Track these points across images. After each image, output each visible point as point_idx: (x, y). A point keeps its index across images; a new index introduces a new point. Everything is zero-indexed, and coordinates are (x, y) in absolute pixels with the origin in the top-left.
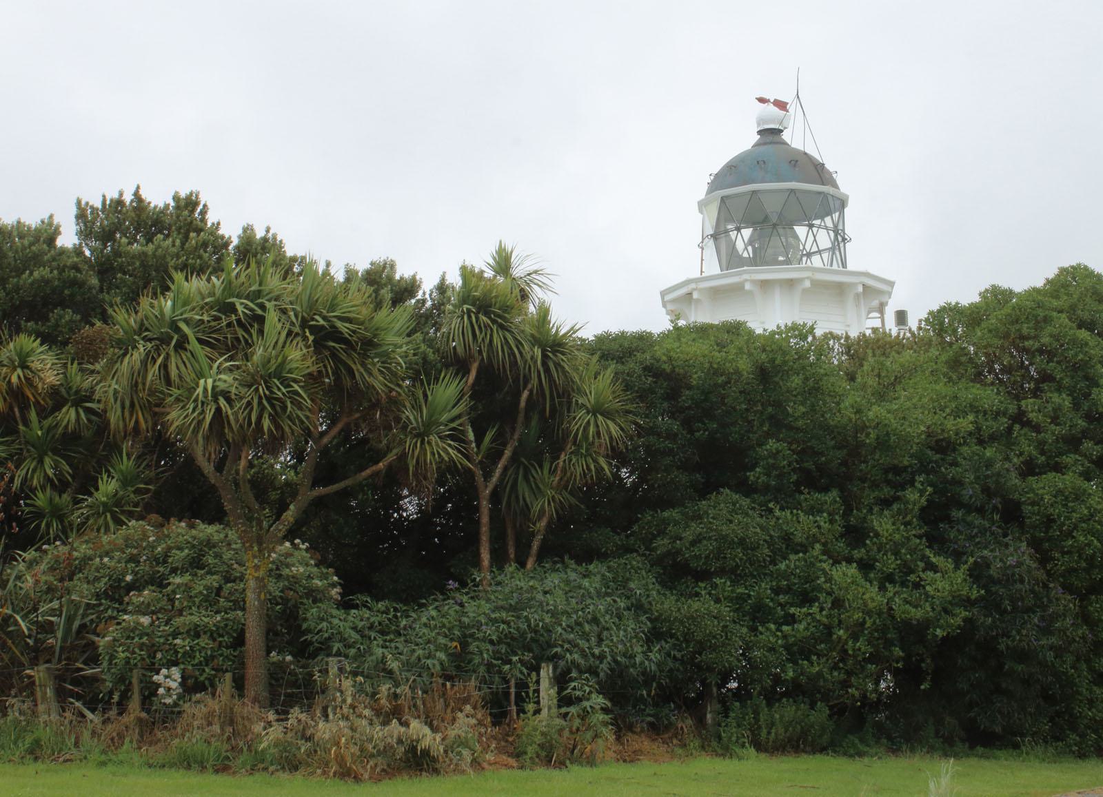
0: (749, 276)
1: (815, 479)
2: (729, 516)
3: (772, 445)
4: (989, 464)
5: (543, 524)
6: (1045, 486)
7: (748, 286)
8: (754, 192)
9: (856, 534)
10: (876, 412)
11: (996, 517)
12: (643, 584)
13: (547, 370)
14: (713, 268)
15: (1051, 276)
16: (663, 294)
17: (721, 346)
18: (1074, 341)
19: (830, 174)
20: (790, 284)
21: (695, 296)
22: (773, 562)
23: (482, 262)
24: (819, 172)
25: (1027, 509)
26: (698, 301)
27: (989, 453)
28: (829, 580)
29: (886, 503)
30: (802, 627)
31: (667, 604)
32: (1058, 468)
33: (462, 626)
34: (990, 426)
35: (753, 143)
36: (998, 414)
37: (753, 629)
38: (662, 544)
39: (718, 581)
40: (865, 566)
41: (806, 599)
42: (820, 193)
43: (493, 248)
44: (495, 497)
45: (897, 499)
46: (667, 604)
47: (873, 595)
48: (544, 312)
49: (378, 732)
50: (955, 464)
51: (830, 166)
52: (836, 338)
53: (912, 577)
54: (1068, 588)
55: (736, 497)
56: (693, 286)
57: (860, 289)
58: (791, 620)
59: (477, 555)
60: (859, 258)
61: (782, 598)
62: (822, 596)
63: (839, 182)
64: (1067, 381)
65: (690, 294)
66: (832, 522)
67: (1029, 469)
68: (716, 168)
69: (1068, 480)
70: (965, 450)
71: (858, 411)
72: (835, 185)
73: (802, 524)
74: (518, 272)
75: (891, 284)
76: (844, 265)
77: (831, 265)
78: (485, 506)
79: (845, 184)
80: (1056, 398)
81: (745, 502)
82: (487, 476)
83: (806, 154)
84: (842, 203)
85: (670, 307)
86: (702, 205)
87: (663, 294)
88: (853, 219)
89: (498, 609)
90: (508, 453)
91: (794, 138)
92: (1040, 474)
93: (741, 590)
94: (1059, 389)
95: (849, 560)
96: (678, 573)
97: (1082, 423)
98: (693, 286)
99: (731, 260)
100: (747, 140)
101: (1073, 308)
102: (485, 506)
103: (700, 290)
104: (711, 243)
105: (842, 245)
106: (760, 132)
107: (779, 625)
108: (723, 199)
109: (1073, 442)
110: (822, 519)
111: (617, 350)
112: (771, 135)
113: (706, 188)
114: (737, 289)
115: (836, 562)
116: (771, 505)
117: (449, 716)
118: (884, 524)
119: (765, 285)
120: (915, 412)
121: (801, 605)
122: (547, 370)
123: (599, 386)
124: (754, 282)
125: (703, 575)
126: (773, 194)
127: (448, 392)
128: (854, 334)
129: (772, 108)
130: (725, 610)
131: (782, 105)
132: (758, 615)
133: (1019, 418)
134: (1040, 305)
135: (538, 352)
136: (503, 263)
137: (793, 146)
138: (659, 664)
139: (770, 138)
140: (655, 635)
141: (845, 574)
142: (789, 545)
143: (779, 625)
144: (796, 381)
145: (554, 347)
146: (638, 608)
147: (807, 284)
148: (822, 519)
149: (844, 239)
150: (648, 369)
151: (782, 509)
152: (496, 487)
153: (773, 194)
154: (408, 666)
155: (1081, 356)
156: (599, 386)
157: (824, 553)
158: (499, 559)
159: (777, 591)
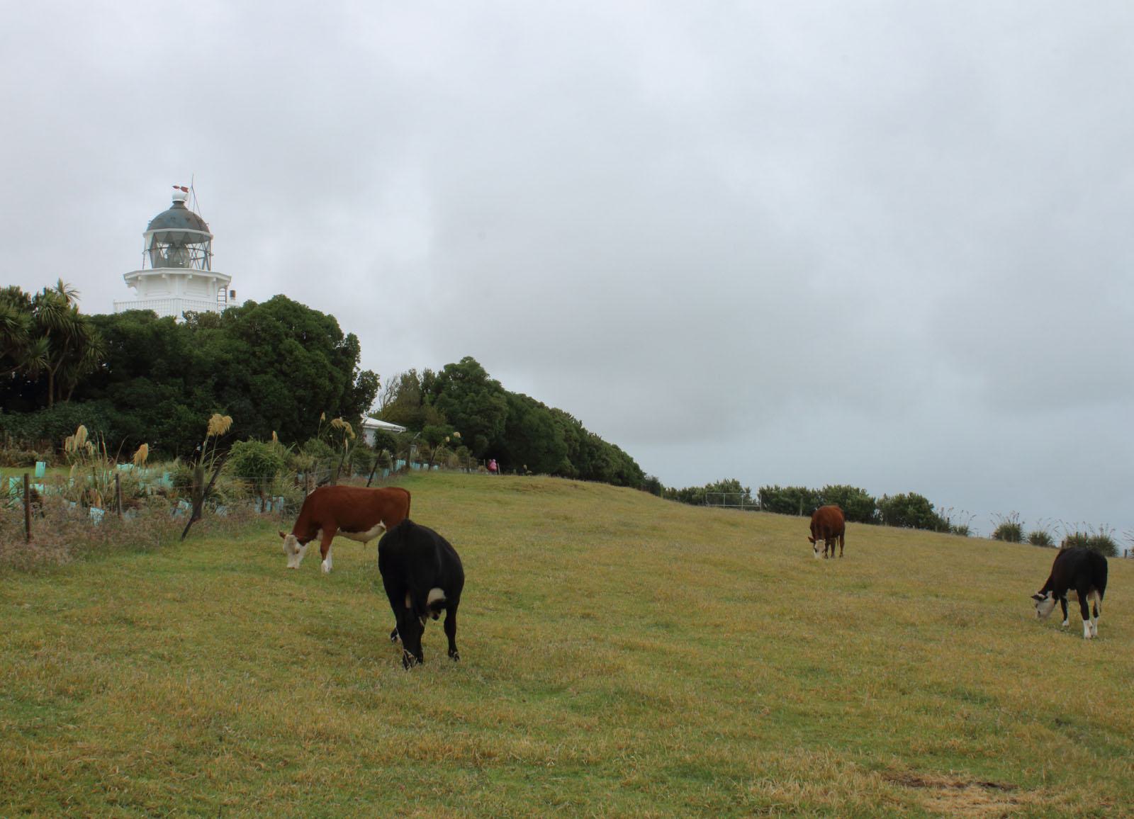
0: (165, 271)
1: (174, 374)
2: (142, 386)
3: (159, 360)
4: (241, 371)
5: (73, 386)
6: (258, 379)
7: (164, 276)
8: (169, 232)
9: (188, 394)
10: (197, 352)
11: (240, 390)
12: (111, 411)
13: (77, 332)
14: (149, 266)
15: (270, 299)
16: (125, 275)
17: (143, 322)
18: (275, 327)
19: (205, 225)
20: (183, 276)
21: (139, 278)
22: (157, 403)
23: (53, 286)
24: (200, 224)
25: (251, 387)
26: (140, 281)
27: (241, 367)
28: (176, 410)
29: (200, 383)
30: (165, 426)
31: (118, 417)
32: (266, 373)
33: (46, 422)
34: (241, 356)
35: (171, 206)
36: (245, 352)
37: (148, 427)
38: (117, 395)
39: (137, 409)
40: (190, 406)
41: (168, 417)
42: (200, 234)
43: (57, 280)
44: (55, 377)
45: (204, 382)
46: (118, 417)
47: (192, 416)
48: (76, 309)
49: (22, 453)
50: (228, 370)
51: (205, 220)
52: (193, 313)
53: (207, 410)
54: (265, 417)
55: (145, 379)
56: (138, 274)
57: (215, 280)
58: (162, 424)
59: (48, 398)
60: (217, 266)
61: (159, 416)
62: (173, 416)
63: (209, 229)
64: (271, 341)
65: (137, 277)
66: (179, 389)
67: (255, 372)
68: (152, 218)
69: (267, 377)
70: (233, 365)
71: (190, 351)
72: (208, 231)
73: (168, 390)
74: (65, 291)
75: (230, 277)
76: (209, 269)
77: (203, 268)
78: (52, 379)
79: (212, 230)
80: (266, 347)
81: (148, 381)
82: (53, 368)
83: (194, 215)
84: (210, 238)
85: (128, 281)
86: (145, 235)
87: (125, 275)
88: (215, 246)
89: (57, 416)
90: (61, 360)
91: (190, 206)
92: (258, 374)
93: (145, 413)
94: (268, 344)
95: (184, 404)
96: (122, 406)
97: (275, 357)
98: (138, 274)
99: (158, 262)
100: (167, 205)
101: (276, 313)
102: (52, 379)
103: (143, 276)
104: (148, 253)
105: (209, 257)
106: (174, 202)
107: (158, 425)
108: (155, 234)
109: (271, 364)
110: (176, 389)
111: (100, 321)
112: (179, 204)
113: (147, 226)
114: (159, 276)
115: (180, 404)
116: (158, 383)
117: (42, 450)
118: (198, 391)
119: (172, 276)
120: (214, 349)
121: (165, 419)
122: (77, 332)
123: (96, 339)
124: (167, 274)
125: (132, 407)
126: (178, 234)
127: (44, 342)
128: (199, 312)
129: (180, 191)
130: (139, 420)
131: (185, 189)
132: (151, 422)
133: (254, 354)
134: (263, 312)
135: (73, 324)
136: (61, 289)
137: (189, 210)
138: (114, 437)
139: (178, 206)
140: (112, 427)
141: (182, 408)
142: (163, 397)
143: (158, 425)
144: (168, 338)
145: (78, 320)
146: (107, 418)
147: (191, 277)
148: (176, 389)
149: (210, 255)
150: (114, 331)
151: (162, 384)
152: (57, 372)
153: (178, 234)
154: (29, 434)
155: (276, 332)
156: (96, 339)
157: (176, 400)
158: (56, 399)
159: (158, 413)
